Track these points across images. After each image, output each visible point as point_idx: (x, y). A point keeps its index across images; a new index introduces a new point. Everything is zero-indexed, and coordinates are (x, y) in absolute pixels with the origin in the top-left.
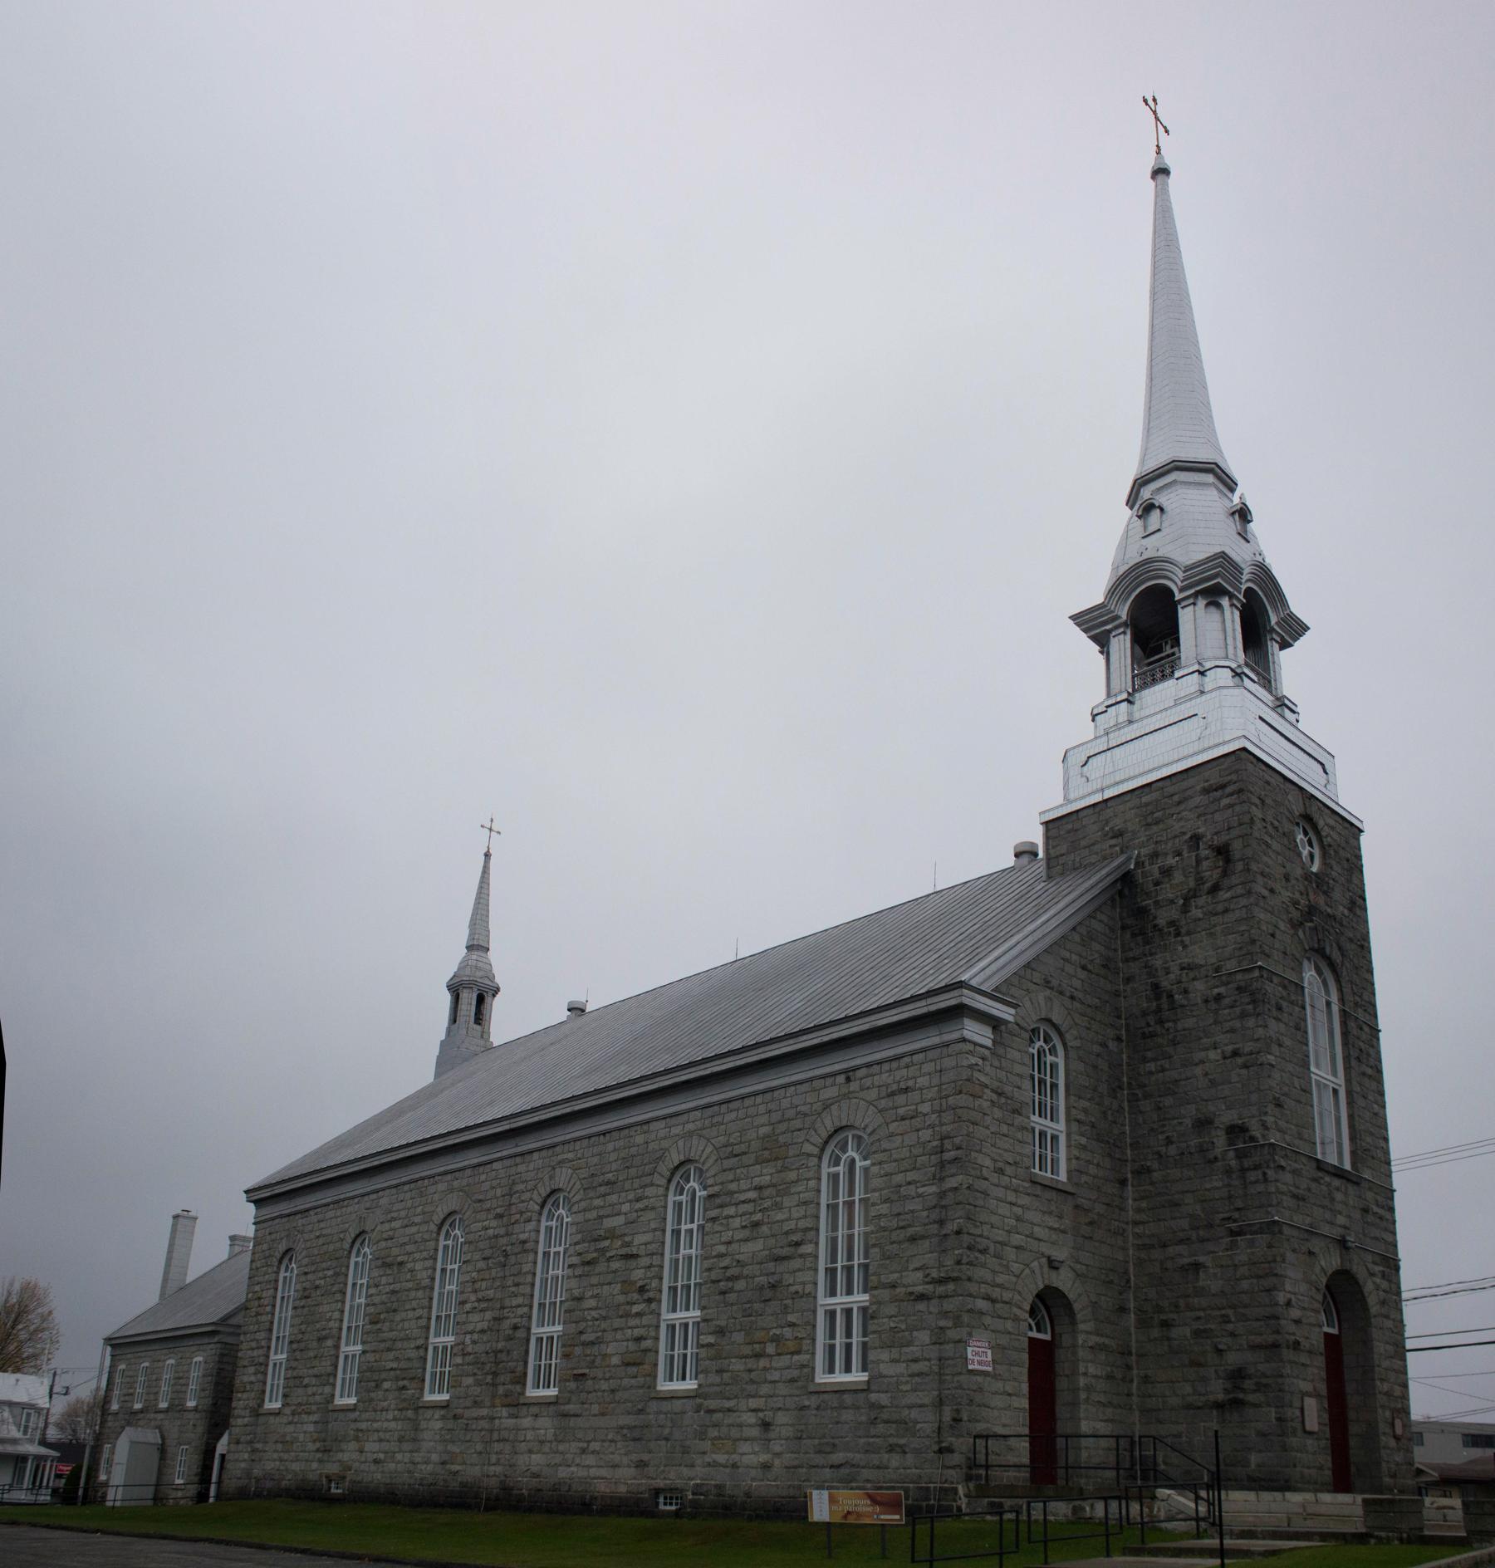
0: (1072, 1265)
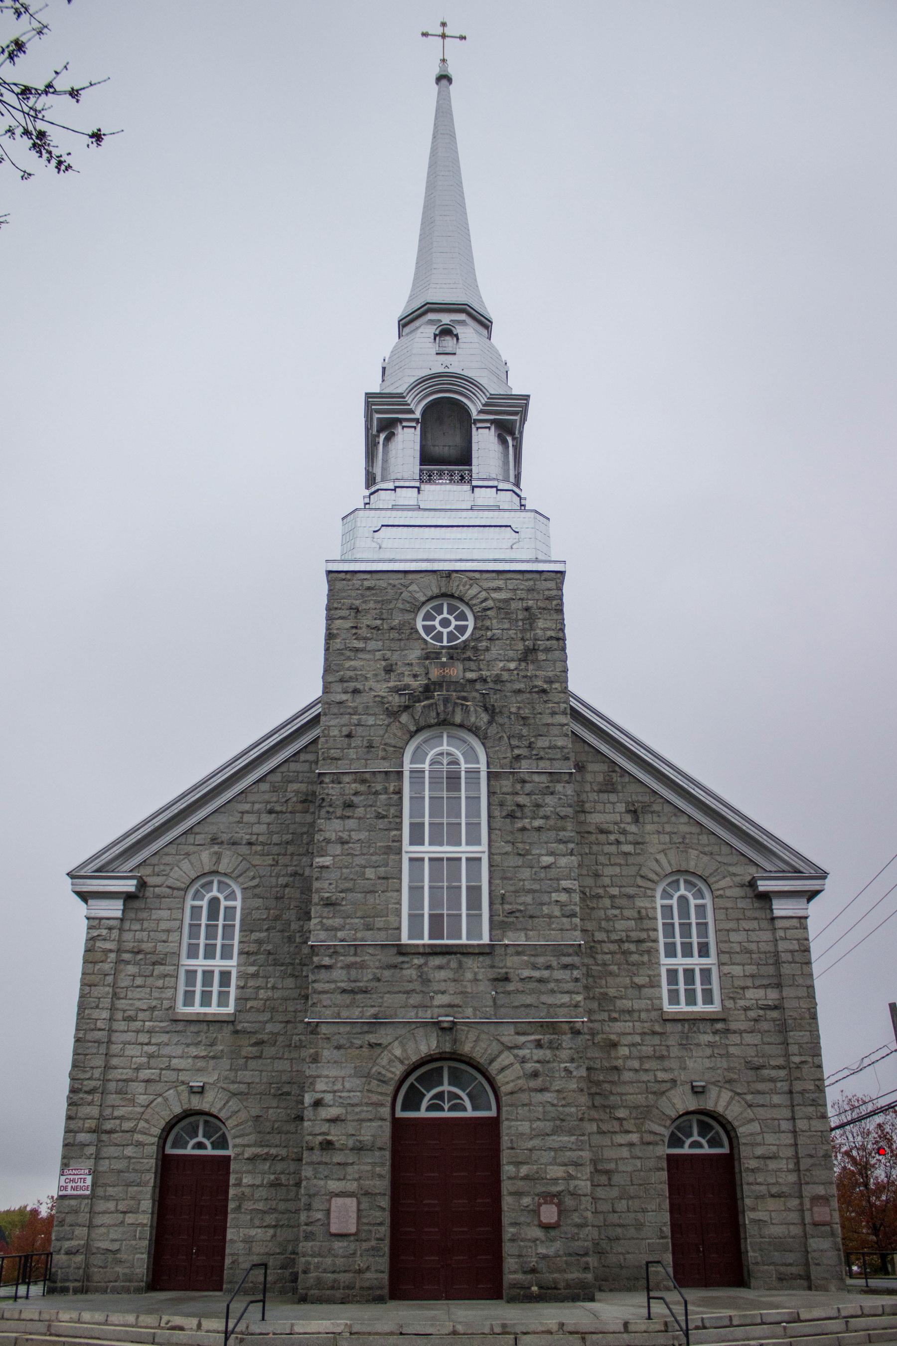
0: (225, 1086)
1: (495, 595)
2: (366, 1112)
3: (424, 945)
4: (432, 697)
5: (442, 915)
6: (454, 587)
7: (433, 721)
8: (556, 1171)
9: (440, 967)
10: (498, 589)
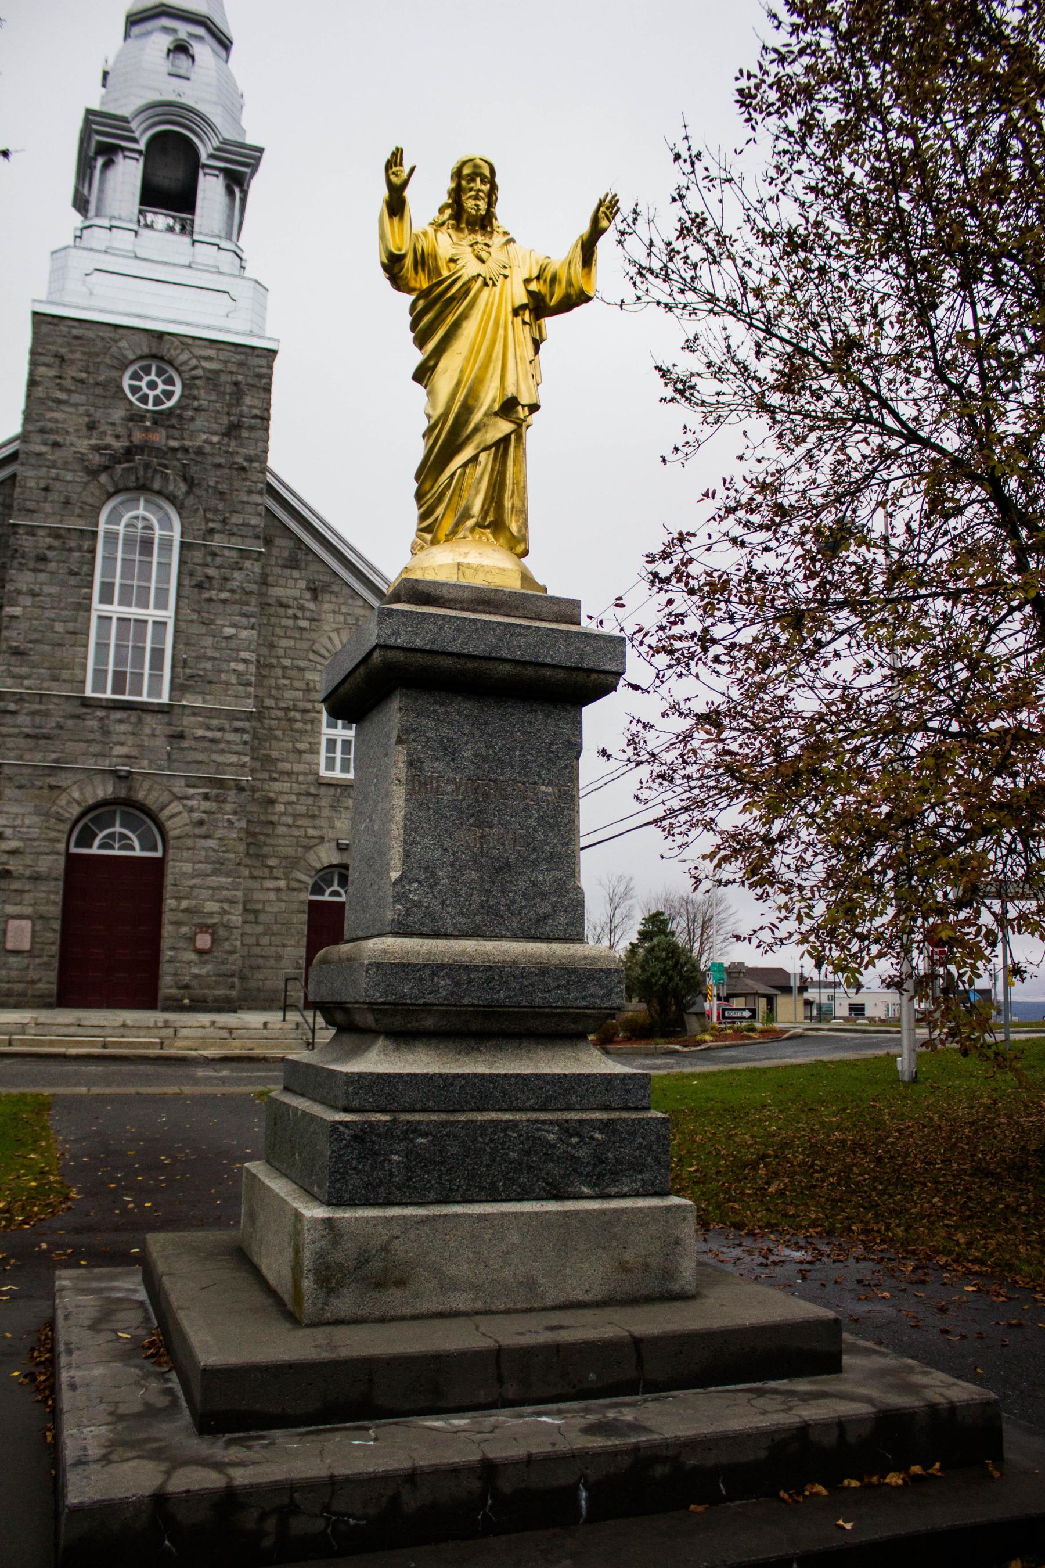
1: (207, 365)
2: (44, 846)
3: (107, 700)
4: (132, 461)
5: (125, 673)
6: (166, 349)
7: (132, 485)
8: (212, 906)
9: (121, 721)
10: (209, 359)
